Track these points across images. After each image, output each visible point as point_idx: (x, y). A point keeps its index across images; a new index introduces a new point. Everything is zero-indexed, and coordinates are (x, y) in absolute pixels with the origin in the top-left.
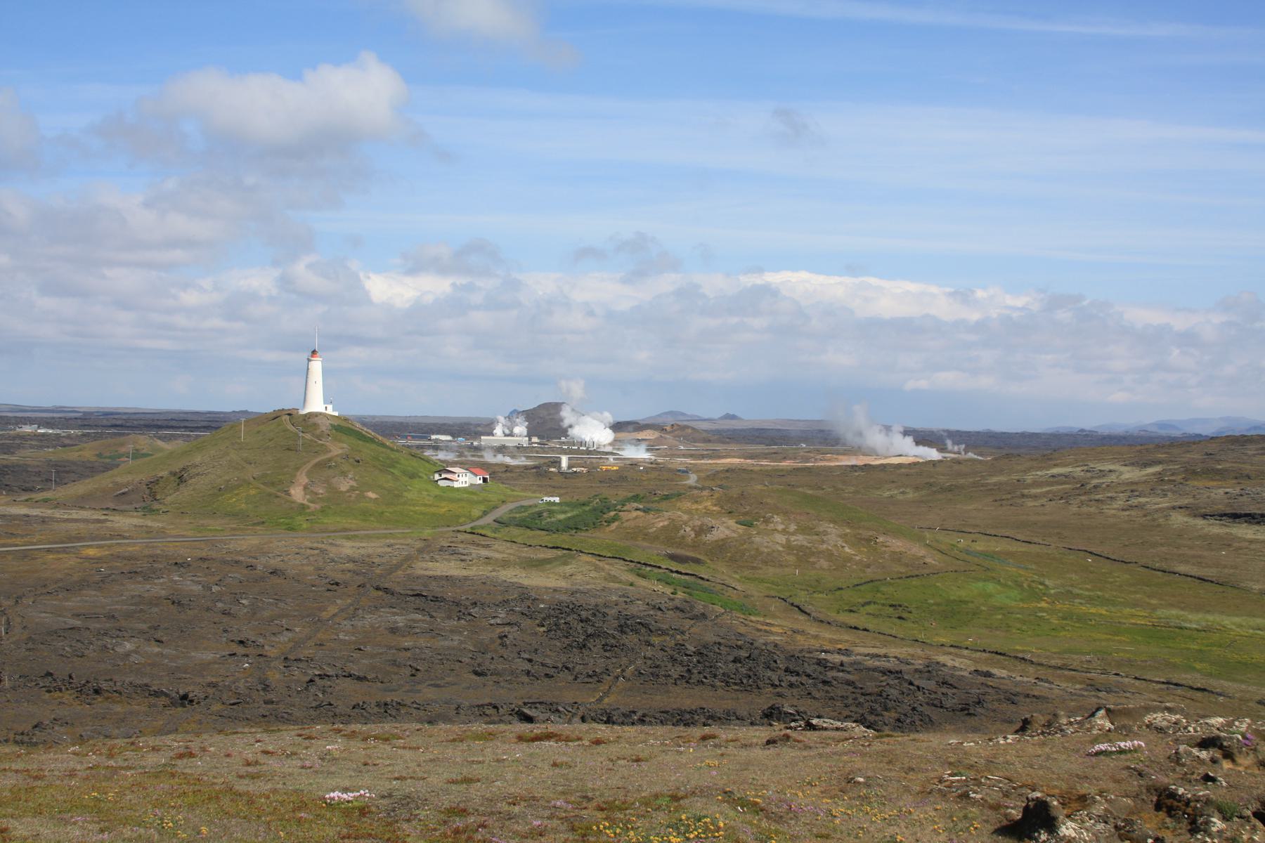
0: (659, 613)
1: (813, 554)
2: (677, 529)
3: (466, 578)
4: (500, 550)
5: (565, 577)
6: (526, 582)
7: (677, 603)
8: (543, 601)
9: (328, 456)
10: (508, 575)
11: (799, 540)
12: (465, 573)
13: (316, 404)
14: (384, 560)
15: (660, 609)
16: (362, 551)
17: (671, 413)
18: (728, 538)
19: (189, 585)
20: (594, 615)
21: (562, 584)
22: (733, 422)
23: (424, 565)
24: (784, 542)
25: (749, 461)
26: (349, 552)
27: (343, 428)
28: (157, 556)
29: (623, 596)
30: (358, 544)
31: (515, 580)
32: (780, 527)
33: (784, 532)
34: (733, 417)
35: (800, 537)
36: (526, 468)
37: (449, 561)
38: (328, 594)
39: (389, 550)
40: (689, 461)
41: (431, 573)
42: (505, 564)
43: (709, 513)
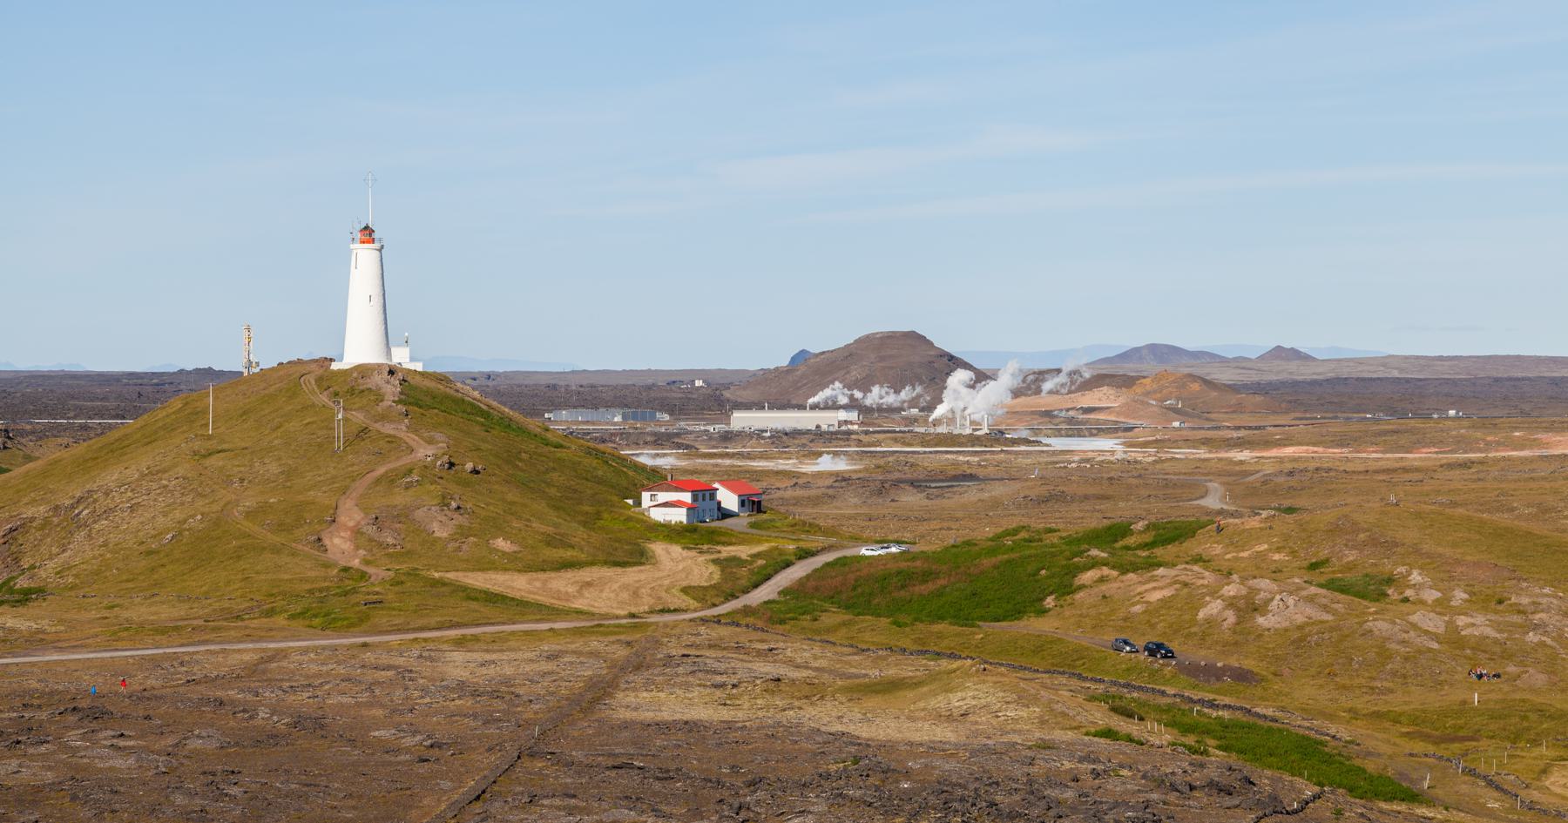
0: (1173, 797)
1: (1507, 656)
2: (1194, 603)
3: (729, 726)
4: (801, 655)
5: (950, 718)
6: (864, 732)
7: (1212, 773)
8: (908, 774)
9: (406, 460)
10: (828, 716)
11: (1477, 625)
12: (725, 714)
13: (359, 347)
14: (539, 689)
15: (1173, 788)
16: (491, 671)
17: (1154, 349)
18: (1311, 622)
19: (109, 757)
20: (1525, 718)
21: (945, 734)
22: (1293, 366)
23: (631, 699)
24: (1441, 630)
25: (1336, 451)
26: (463, 674)
27: (428, 398)
28: (31, 693)
29: (1084, 759)
30: (479, 657)
31: (837, 728)
32: (1431, 595)
33: (1442, 606)
34: (1295, 354)
35: (1480, 619)
36: (842, 479)
37: (687, 686)
38: (423, 769)
39: (550, 666)
40: (1202, 453)
41: (648, 716)
42: (813, 691)
43: (1261, 566)
